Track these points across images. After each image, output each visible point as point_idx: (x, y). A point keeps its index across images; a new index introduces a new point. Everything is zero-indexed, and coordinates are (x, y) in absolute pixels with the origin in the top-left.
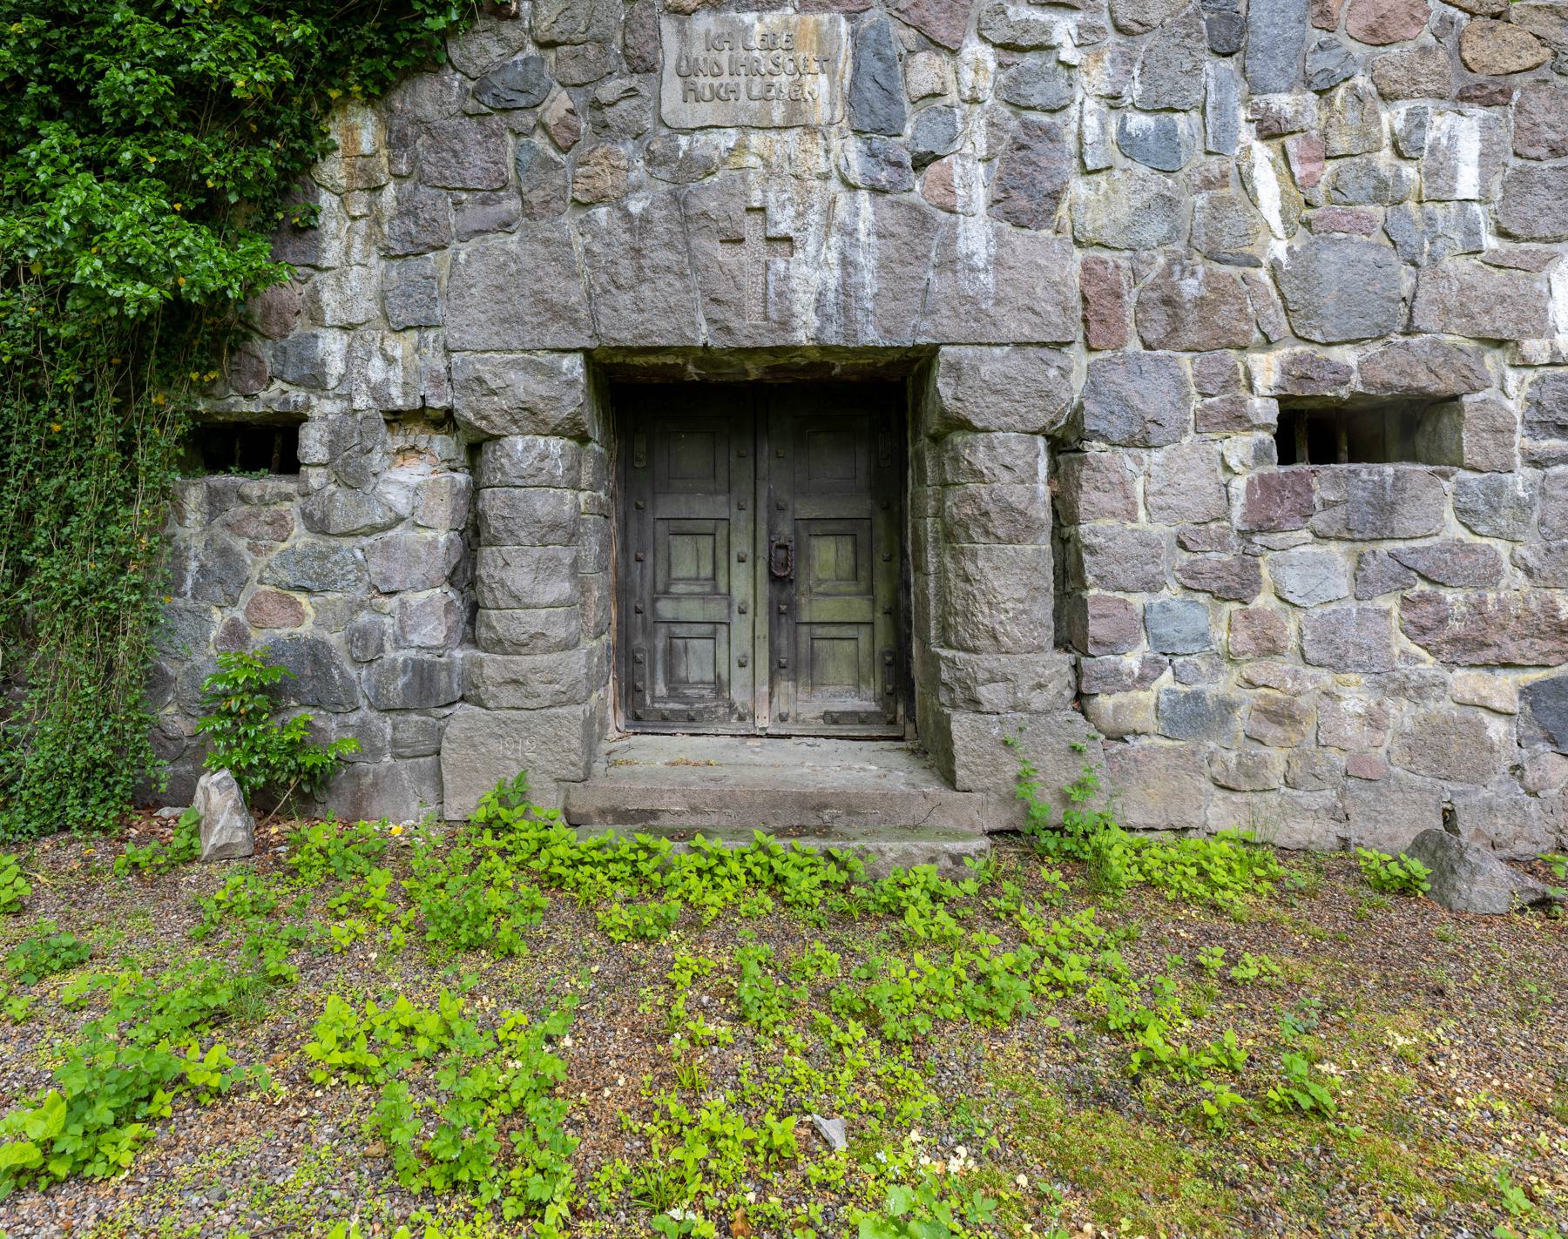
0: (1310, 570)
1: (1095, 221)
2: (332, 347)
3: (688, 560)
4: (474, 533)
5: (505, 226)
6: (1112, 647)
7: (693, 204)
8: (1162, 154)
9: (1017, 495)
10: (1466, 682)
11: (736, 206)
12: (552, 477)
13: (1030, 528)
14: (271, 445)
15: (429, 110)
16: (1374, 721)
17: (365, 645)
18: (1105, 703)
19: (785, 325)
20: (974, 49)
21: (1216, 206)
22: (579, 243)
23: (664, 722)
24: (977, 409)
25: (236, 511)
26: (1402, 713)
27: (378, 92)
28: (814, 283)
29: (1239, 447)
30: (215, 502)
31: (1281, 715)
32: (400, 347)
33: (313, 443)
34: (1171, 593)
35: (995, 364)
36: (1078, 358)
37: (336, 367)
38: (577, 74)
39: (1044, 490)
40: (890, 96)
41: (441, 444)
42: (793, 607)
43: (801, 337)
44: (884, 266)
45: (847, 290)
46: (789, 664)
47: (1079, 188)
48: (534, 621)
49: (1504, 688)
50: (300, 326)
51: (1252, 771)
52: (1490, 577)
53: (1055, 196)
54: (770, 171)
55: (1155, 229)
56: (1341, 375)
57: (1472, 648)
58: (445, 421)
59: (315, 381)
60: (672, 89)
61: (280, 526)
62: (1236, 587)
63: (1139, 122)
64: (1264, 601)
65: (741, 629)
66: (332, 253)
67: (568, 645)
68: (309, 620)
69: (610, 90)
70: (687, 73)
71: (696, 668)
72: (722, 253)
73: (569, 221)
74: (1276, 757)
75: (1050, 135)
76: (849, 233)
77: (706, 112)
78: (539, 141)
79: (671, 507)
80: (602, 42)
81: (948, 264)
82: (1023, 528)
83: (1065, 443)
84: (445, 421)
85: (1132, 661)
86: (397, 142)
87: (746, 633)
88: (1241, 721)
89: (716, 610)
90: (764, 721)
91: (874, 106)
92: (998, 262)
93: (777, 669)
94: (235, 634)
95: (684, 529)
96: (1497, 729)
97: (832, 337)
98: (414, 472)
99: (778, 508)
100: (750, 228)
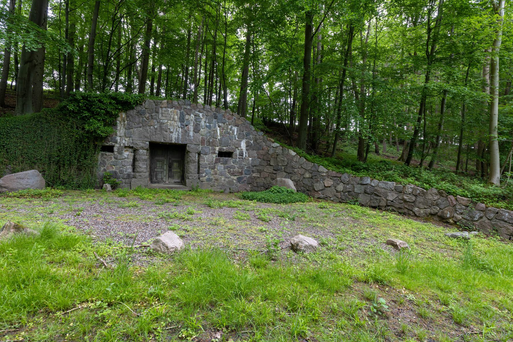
0: (220, 167)
1: (203, 133)
2: (118, 139)
3: (159, 164)
4: (135, 160)
5: (140, 127)
6: (202, 173)
7: (162, 128)
8: (209, 127)
9: (194, 159)
10: (232, 177)
11: (167, 128)
12: (144, 154)
13: (195, 162)
14: (110, 149)
15: (132, 114)
16: (224, 180)
17: (121, 172)
18: (201, 179)
19: (172, 140)
20: (192, 115)
21: (214, 133)
22: (149, 130)
23: (155, 183)
24: (190, 150)
25: (105, 156)
26: (227, 180)
27: (126, 111)
28: (175, 136)
29: (214, 156)
30: (102, 155)
31: (216, 180)
32: (127, 139)
33: (115, 149)
34: (208, 169)
35: (192, 146)
36: (201, 146)
37: (119, 141)
38: (149, 112)
39: (197, 158)
40: (183, 119)
41: (130, 150)
42: (171, 170)
43: (173, 142)
44: (182, 135)
45: (178, 138)
46: (170, 176)
47: (202, 130)
48: (142, 169)
49: (235, 178)
50: (114, 136)
51: (214, 185)
52: (235, 168)
53: (199, 130)
54: (171, 125)
55: (208, 135)
56: (224, 150)
57: (233, 174)
58: (130, 147)
59: (116, 142)
60: (160, 115)
61: (111, 158)
62: (213, 168)
63: (207, 124)
64: (216, 169)
65: (165, 172)
66: (119, 128)
67: (145, 172)
68: (114, 169)
69: (153, 114)
70: (162, 114)
71: (159, 177)
72: (165, 133)
73: (148, 128)
74: (216, 183)
75: (199, 124)
76: (179, 132)
77: (164, 118)
78: (145, 118)
79: (157, 158)
80: (153, 109)
81: (189, 136)
82: (195, 162)
83: (199, 154)
84: (132, 147)
85: (204, 175)
86: (127, 117)
87: (166, 173)
88: (213, 180)
89: (162, 170)
90: (167, 183)
91: (182, 119)
92: (193, 136)
93: (169, 177)
94: (105, 170)
95: (158, 161)
96: (235, 181)
97: (176, 142)
98: (127, 153)
99: (170, 159)
100: (168, 130)
